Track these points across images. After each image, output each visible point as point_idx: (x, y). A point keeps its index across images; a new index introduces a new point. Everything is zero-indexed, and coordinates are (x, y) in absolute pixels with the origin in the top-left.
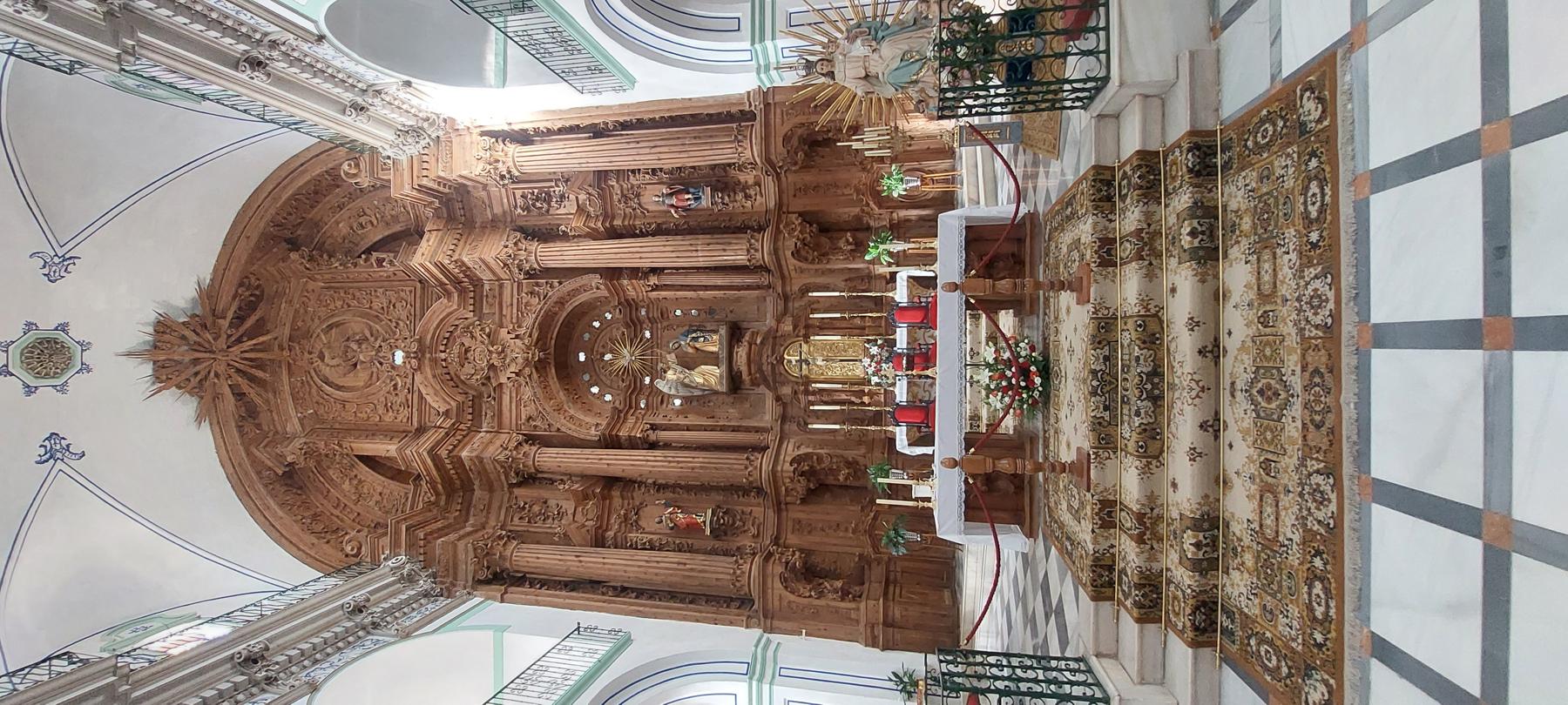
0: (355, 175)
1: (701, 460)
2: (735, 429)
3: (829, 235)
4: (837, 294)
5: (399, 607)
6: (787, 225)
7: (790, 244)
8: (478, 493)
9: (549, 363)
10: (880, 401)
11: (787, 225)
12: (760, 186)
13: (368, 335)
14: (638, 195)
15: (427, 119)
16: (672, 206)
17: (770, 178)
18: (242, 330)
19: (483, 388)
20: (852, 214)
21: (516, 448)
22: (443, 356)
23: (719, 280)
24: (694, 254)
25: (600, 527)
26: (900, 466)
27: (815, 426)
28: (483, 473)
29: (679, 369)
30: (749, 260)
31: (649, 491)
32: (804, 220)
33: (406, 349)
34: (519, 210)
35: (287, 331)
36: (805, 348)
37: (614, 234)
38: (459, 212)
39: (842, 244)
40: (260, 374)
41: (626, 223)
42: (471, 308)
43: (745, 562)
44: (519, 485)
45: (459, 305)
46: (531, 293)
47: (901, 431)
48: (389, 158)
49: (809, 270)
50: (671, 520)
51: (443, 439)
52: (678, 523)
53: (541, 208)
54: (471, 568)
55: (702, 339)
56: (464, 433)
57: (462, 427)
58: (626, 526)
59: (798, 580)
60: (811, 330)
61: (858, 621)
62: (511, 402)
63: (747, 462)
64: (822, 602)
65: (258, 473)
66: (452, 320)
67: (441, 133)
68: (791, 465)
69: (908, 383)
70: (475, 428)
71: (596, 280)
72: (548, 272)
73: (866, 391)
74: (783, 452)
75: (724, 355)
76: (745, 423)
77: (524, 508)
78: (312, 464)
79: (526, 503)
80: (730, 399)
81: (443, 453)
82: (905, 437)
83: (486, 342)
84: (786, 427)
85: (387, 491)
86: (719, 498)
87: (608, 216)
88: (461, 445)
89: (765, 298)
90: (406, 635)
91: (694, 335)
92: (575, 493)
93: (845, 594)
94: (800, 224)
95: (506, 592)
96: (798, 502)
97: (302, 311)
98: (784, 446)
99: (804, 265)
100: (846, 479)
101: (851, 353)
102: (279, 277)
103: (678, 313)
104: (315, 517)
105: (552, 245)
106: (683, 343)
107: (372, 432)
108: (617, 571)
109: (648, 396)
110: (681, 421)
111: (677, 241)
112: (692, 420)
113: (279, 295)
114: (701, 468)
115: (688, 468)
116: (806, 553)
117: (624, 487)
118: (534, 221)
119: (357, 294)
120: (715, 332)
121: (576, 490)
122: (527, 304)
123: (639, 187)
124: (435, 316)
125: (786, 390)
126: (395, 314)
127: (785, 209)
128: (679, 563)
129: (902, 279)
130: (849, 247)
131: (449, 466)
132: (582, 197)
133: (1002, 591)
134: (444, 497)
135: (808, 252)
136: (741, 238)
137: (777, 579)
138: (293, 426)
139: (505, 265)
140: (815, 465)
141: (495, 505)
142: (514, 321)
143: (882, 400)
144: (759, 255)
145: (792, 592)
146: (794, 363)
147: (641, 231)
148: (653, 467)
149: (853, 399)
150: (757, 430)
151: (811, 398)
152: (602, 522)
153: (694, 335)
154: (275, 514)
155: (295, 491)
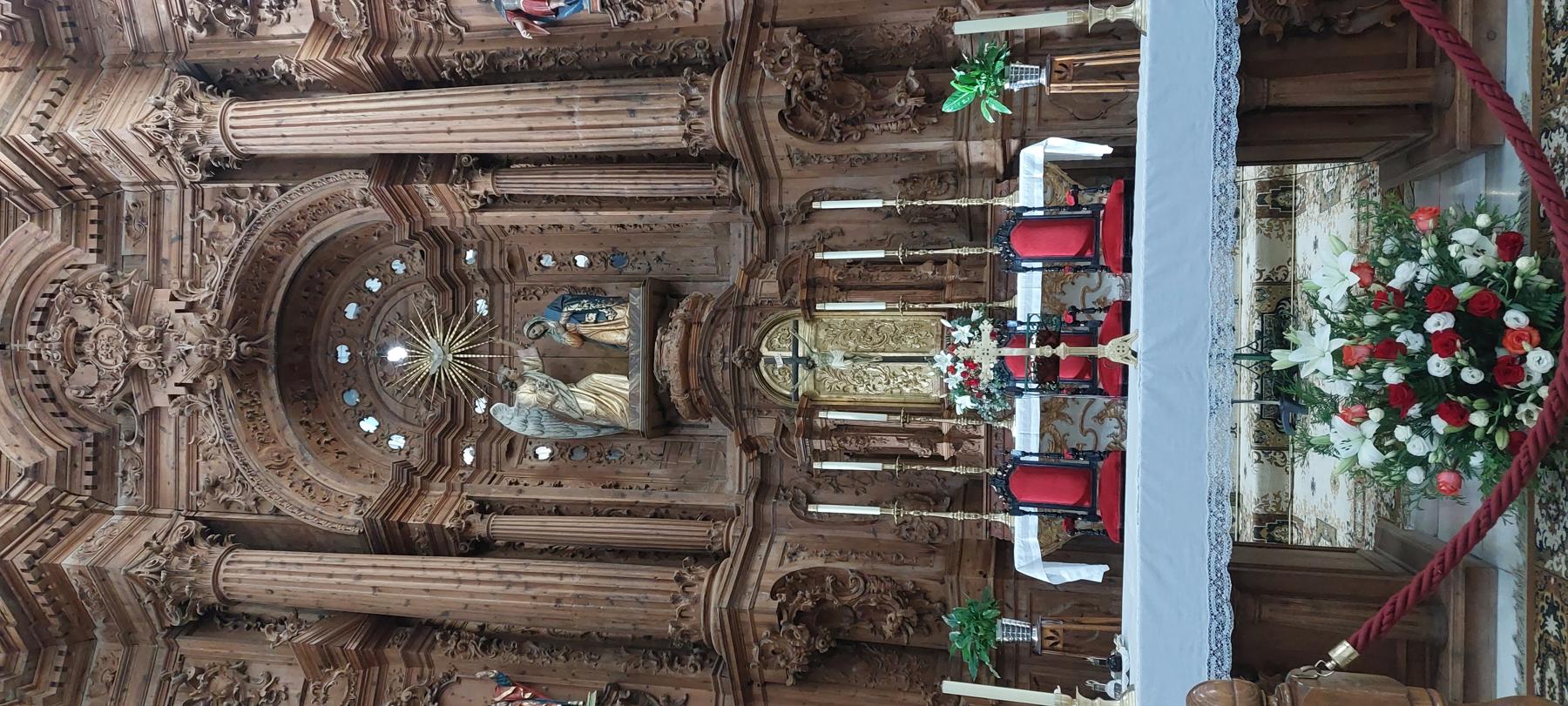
1: (576, 580)
2: (660, 513)
3: (869, 78)
4: (878, 204)
6: (771, 50)
7: (774, 93)
8: (102, 647)
9: (264, 366)
10: (977, 455)
11: (771, 50)
19: (120, 419)
21: (179, 548)
22: (31, 347)
24: (566, 122)
26: (1024, 607)
27: (823, 509)
28: (111, 602)
29: (543, 378)
30: (687, 136)
31: (466, 646)
32: (808, 40)
34: (190, 28)
36: (806, 331)
37: (392, 79)
38: (64, 33)
39: (894, 96)
41: (420, 54)
42: (93, 244)
44: (190, 629)
45: (65, 237)
46: (221, 212)
47: (1025, 525)
49: (820, 158)
51: (20, 527)
53: (237, 22)
55: (592, 316)
56: (72, 516)
60: (820, 291)
62: (177, 449)
63: (676, 587)
66: (53, 268)
68: (773, 596)
69: (1045, 409)
70: (99, 503)
71: (358, 183)
72: (253, 165)
73: (945, 429)
74: (757, 566)
75: (638, 351)
76: (679, 499)
77: (194, 682)
79: (200, 671)
80: (655, 447)
82: (1034, 540)
83: (122, 317)
84: (768, 509)
86: (614, 665)
87: (379, 38)
88: (65, 541)
89: (728, 224)
91: (575, 307)
94: (800, 47)
96: (790, 681)
98: (762, 551)
99: (808, 147)
100: (899, 630)
101: (910, 346)
105: (260, 104)
106: (551, 324)
109: (480, 440)
110: (548, 494)
111: (528, 94)
112: (573, 491)
115: (548, 599)
117: (414, 636)
118: (225, 52)
120: (621, 301)
122: (214, 236)
124: (15, 259)
125: (765, 427)
127: (766, 18)
129: (1033, 164)
130: (911, 102)
131: (34, 588)
134: (23, 657)
135: (816, 115)
136: (670, 85)
139: (159, 147)
140: (829, 596)
142: (186, 272)
143: (982, 451)
144: (707, 125)
146: (780, 364)
147: (453, 73)
148: (472, 595)
149: (915, 448)
150: (708, 515)
151: (818, 444)
153: (575, 307)
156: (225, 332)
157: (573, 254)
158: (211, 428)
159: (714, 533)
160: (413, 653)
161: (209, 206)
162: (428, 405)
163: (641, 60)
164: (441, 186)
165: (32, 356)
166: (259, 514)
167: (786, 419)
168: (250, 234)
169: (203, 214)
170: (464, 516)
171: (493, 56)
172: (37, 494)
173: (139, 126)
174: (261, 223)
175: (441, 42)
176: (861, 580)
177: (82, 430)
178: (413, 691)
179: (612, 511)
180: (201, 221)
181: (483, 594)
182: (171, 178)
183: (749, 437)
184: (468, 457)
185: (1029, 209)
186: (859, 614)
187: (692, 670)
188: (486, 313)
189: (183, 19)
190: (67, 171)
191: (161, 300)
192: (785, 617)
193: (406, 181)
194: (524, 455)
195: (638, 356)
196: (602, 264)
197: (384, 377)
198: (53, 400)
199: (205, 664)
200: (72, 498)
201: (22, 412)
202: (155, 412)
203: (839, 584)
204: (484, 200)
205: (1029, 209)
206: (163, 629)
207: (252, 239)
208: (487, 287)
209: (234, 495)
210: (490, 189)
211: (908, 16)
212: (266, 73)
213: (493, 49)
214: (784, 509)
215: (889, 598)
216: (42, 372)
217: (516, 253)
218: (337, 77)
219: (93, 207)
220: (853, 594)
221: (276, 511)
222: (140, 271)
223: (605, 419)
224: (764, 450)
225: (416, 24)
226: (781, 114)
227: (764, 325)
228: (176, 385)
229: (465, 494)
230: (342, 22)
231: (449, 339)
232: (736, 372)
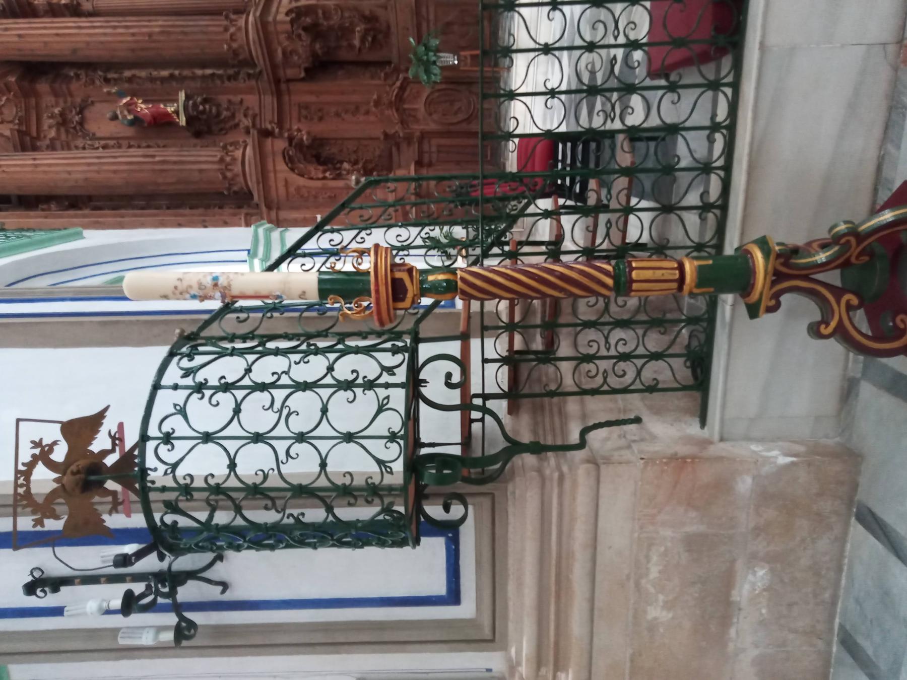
31: (93, 82)
50: (129, 112)
52: (139, 115)
58: (67, 132)
59: (309, 162)
63: (225, 23)
96: (303, 75)
108: (57, 173)
115: (143, 34)
133: (558, 119)
137: (280, 160)
140: (321, 21)
145: (302, 175)
152: (28, 126)
160: (57, 85)
186: (340, 34)
192: (295, 26)
215: (356, 20)
220: (335, 20)
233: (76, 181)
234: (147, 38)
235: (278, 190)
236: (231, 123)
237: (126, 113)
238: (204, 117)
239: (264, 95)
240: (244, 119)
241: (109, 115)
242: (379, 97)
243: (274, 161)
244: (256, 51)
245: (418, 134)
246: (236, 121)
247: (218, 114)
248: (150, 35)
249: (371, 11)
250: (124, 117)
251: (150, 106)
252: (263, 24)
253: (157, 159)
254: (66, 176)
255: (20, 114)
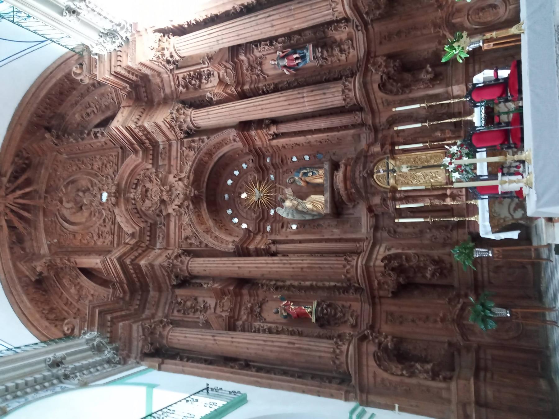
0: (80, 74)
5: (87, 367)
7: (376, 78)
8: (152, 293)
12: (352, 41)
13: (90, 186)
14: (261, 64)
15: (119, 25)
16: (285, 66)
17: (360, 32)
18: (16, 184)
19: (158, 219)
20: (431, 51)
23: (322, 123)
24: (302, 100)
25: (233, 317)
28: (155, 277)
30: (344, 100)
31: (270, 289)
33: (109, 191)
34: (181, 88)
35: (44, 188)
37: (243, 96)
40: (26, 214)
43: (344, 344)
45: (143, 159)
47: (483, 204)
48: (96, 54)
50: (285, 310)
54: (140, 344)
56: (144, 249)
57: (143, 245)
58: (252, 317)
59: (390, 360)
61: (449, 401)
63: (344, 262)
64: (413, 381)
65: (19, 279)
67: (129, 35)
68: (382, 261)
70: (151, 246)
71: (232, 133)
78: (52, 274)
80: (334, 223)
81: (128, 261)
83: (159, 184)
84: (379, 235)
85: (96, 294)
86: (325, 294)
87: (239, 83)
88: (141, 257)
90: (84, 385)
91: (305, 171)
92: (215, 291)
93: (434, 376)
95: (163, 363)
96: (390, 295)
97: (54, 175)
100: (433, 275)
102: (40, 153)
103: (295, 159)
104: (52, 310)
106: (296, 178)
107: (88, 251)
113: (41, 164)
114: (308, 267)
115: (298, 268)
116: (399, 341)
118: (193, 95)
119: (85, 160)
121: (216, 288)
123: (261, 58)
126: (105, 172)
127: (372, 55)
128: (289, 343)
132: (222, 72)
135: (392, 85)
138: (45, 250)
140: (404, 263)
141: (163, 301)
142: (178, 168)
144: (351, 94)
145: (386, 370)
148: (271, 268)
152: (234, 313)
153: (305, 171)
154: (26, 306)
155: (41, 292)
156: (190, 187)
157: (303, 156)
158: (186, 219)
159: (358, 245)
160: (252, 291)
161: (185, 145)
162: (255, 212)
163: (327, 78)
164: (259, 131)
165: (132, 199)
166: (201, 247)
167: (385, 195)
168: (198, 154)
169: (184, 149)
170: (268, 245)
171: (276, 84)
172: (133, 242)
173: (166, 119)
174: (202, 150)
175: (259, 81)
176: (417, 256)
177: (146, 222)
178: (252, 304)
179: (320, 241)
180: (183, 151)
181: (275, 267)
182: (174, 138)
183: (370, 205)
184: (268, 228)
185: (478, 84)
186: (416, 270)
187: (352, 294)
188: (273, 179)
189: (178, 86)
190: (144, 138)
191: (171, 178)
192: (387, 269)
193: (248, 130)
194: (287, 227)
195: (327, 186)
196: (314, 158)
197: (240, 203)
198: (138, 213)
199: (184, 298)
200: (143, 244)
201: (129, 217)
202: (169, 215)
203: (408, 259)
204: (273, 136)
205: (478, 84)
206: (171, 285)
207: (199, 156)
208: (274, 170)
209: (193, 241)
210: (276, 131)
211: (426, 46)
212: (203, 101)
213: (276, 81)
214: (385, 234)
215: (428, 263)
216: (135, 204)
217: (284, 157)
218: (226, 98)
219: (151, 150)
220: (414, 262)
221: (206, 245)
222: (165, 169)
223: (316, 211)
224: (376, 212)
225: (251, 77)
226: (379, 85)
227: (375, 161)
228: (175, 205)
229: (268, 238)
230: (227, 78)
231: (262, 188)
232: (365, 179)
233: (251, 354)
234: (300, 270)
235: (369, 379)
236: (342, 320)
237: (283, 311)
238: (327, 316)
239: (364, 303)
240: (350, 318)
241: (274, 311)
242: (444, 315)
243: (367, 359)
244: (356, 103)
245: (475, 345)
246: (346, 319)
247: (336, 314)
248: (302, 268)
249: (439, 257)
250: (282, 314)
251: (297, 307)
252: (367, 267)
253: (296, 346)
254: (246, 350)
255: (232, 306)
